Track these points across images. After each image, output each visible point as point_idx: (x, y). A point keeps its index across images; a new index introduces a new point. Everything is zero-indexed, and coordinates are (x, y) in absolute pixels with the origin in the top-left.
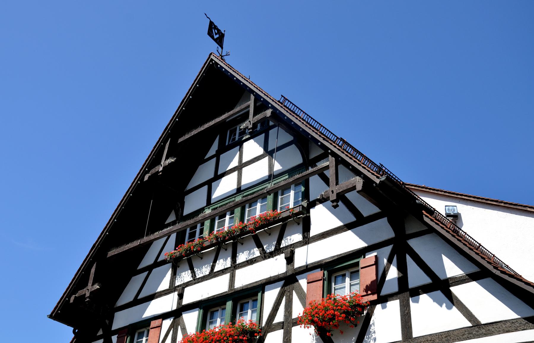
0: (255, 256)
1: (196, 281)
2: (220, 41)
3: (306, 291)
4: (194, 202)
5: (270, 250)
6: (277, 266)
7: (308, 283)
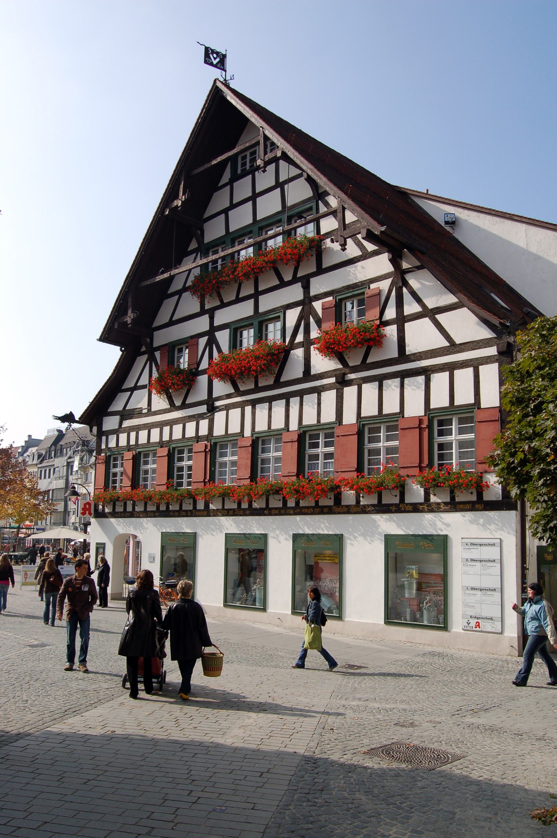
1: (223, 305)
2: (221, 65)
3: (321, 317)
4: (214, 230)
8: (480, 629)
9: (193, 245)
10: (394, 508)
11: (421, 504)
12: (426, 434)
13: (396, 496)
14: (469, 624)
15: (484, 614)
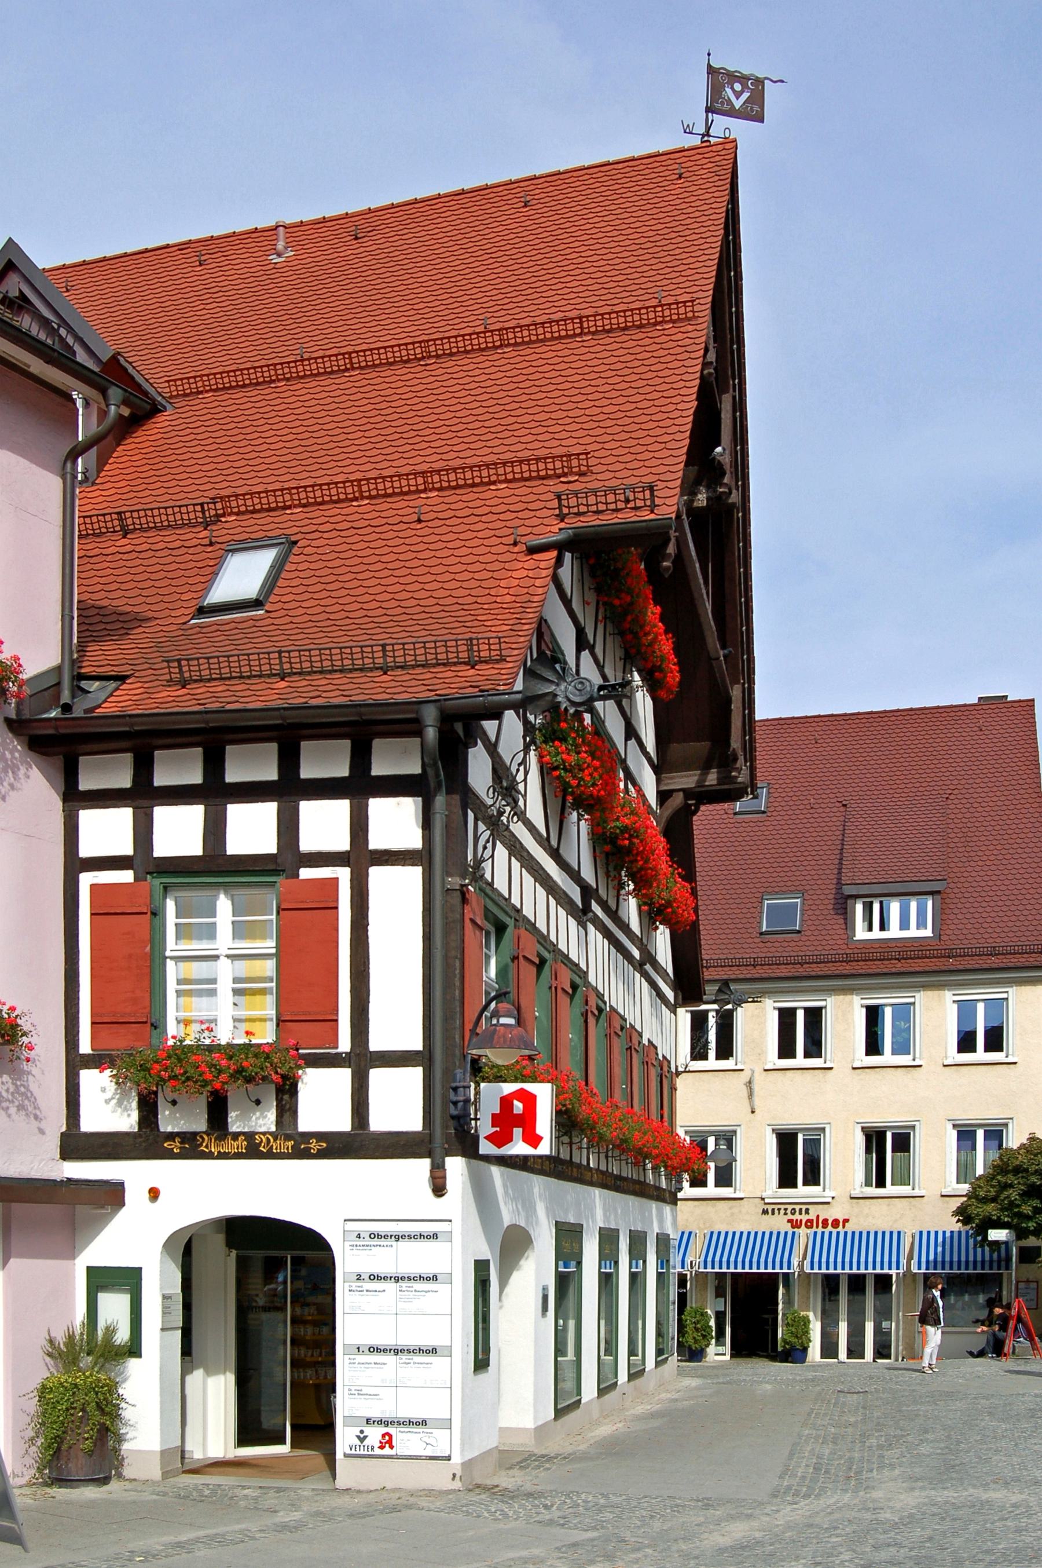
8: (392, 1452)
10: (314, 1146)
14: (362, 1439)
15: (404, 1414)
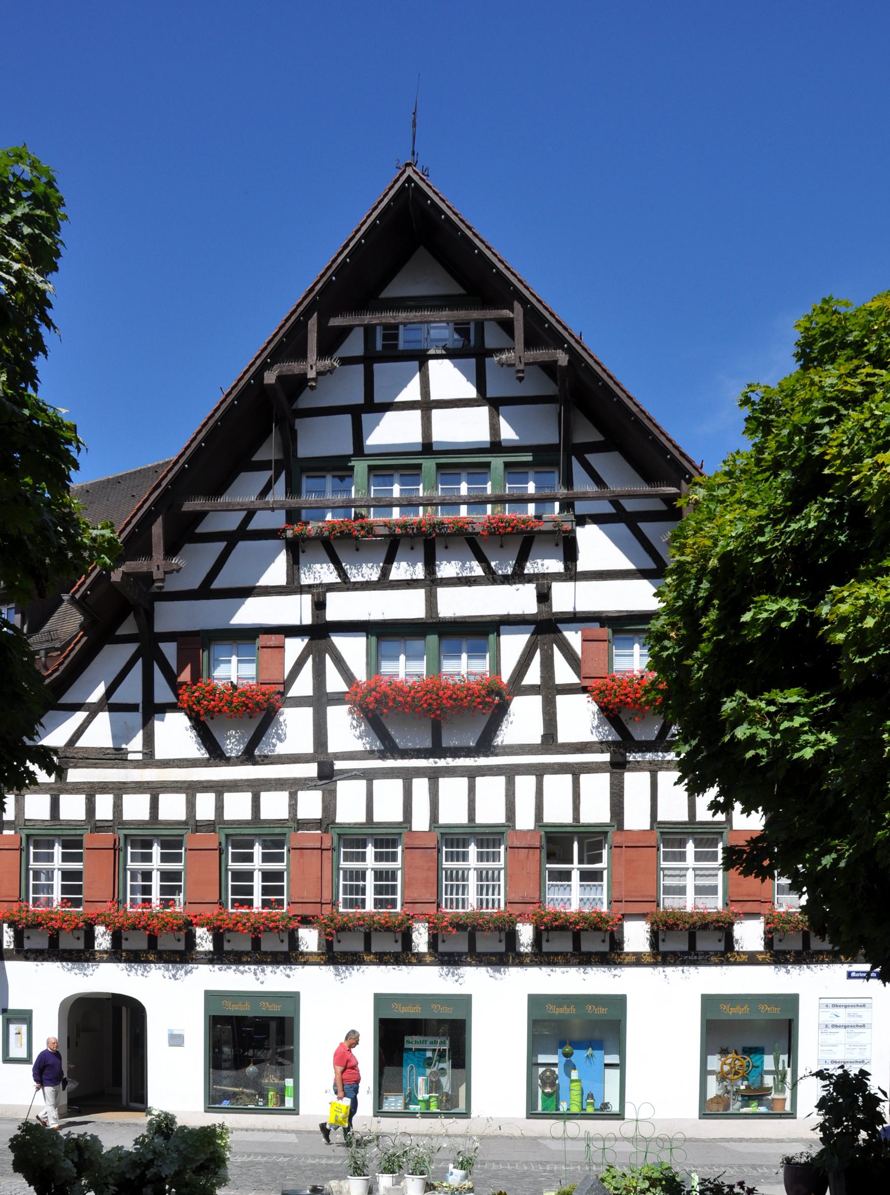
0: (473, 574)
1: (346, 585)
5: (505, 571)
6: (521, 600)
7: (584, 640)
9: (269, 451)
11: (760, 953)
12: (24, 854)
13: (78, 938)
